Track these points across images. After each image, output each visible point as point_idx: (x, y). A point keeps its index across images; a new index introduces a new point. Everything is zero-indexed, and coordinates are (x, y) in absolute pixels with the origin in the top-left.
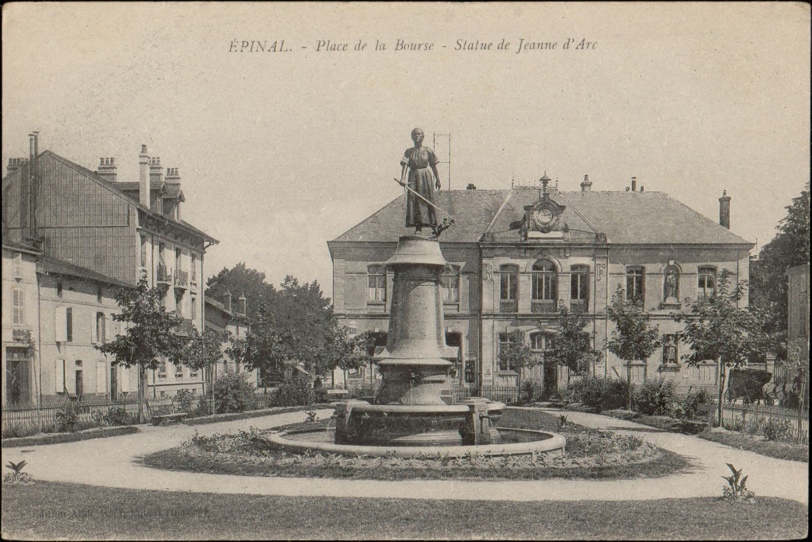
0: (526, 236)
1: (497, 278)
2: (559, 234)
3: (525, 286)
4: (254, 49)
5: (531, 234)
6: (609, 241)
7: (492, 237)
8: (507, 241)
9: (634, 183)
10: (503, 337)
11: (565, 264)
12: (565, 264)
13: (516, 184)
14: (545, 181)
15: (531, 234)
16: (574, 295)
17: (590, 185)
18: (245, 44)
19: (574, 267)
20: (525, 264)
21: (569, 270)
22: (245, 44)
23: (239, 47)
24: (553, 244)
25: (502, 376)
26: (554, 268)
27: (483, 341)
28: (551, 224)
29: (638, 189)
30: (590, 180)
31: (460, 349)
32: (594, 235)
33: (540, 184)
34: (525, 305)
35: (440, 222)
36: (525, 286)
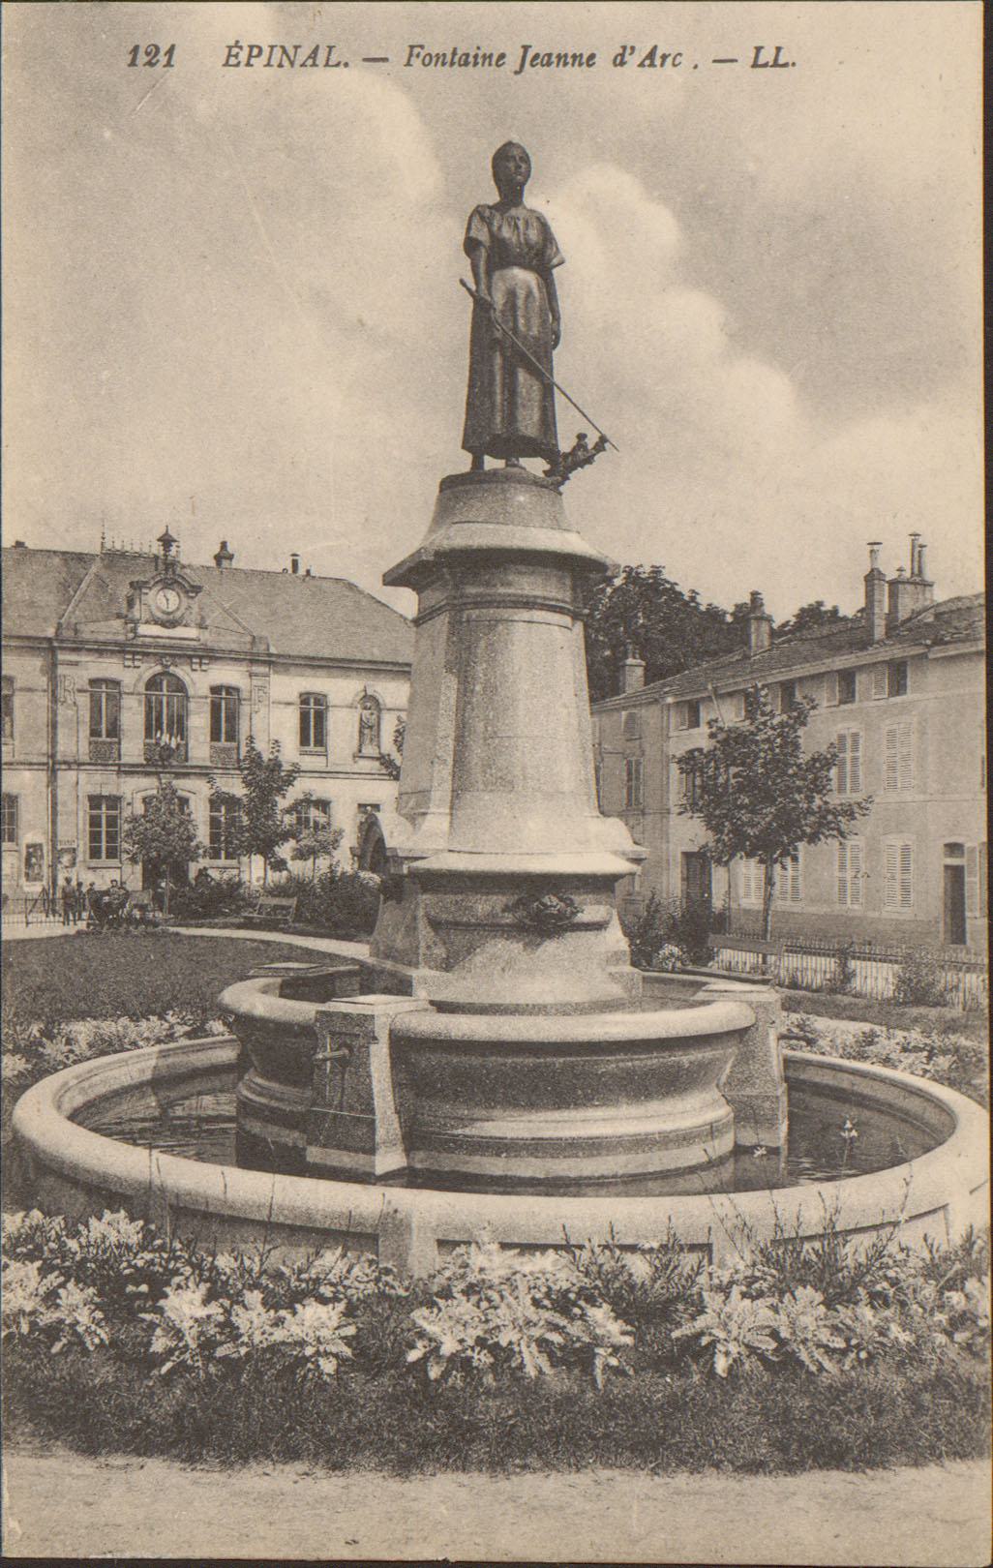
0: (134, 630)
1: (84, 700)
2: (192, 632)
3: (133, 716)
4: (275, 61)
5: (143, 629)
6: (273, 650)
7: (76, 631)
8: (101, 638)
9: (295, 564)
10: (95, 801)
11: (200, 681)
12: (200, 681)
13: (108, 545)
14: (167, 541)
15: (143, 629)
16: (215, 735)
17: (231, 557)
18: (255, 51)
19: (215, 690)
20: (132, 676)
21: (207, 692)
22: (255, 51)
23: (243, 56)
24: (181, 648)
25: (94, 869)
26: (180, 687)
27: (59, 808)
28: (178, 614)
29: (302, 571)
30: (230, 549)
31: (861, 668)
32: (248, 639)
33: (157, 549)
34: (133, 748)
35: (565, 445)
36: (133, 716)
